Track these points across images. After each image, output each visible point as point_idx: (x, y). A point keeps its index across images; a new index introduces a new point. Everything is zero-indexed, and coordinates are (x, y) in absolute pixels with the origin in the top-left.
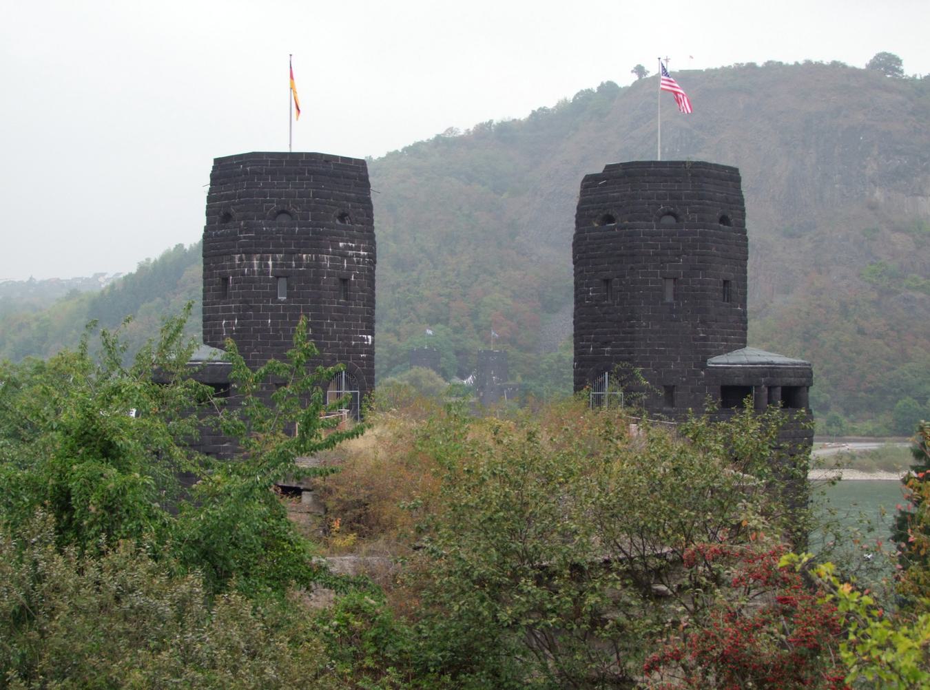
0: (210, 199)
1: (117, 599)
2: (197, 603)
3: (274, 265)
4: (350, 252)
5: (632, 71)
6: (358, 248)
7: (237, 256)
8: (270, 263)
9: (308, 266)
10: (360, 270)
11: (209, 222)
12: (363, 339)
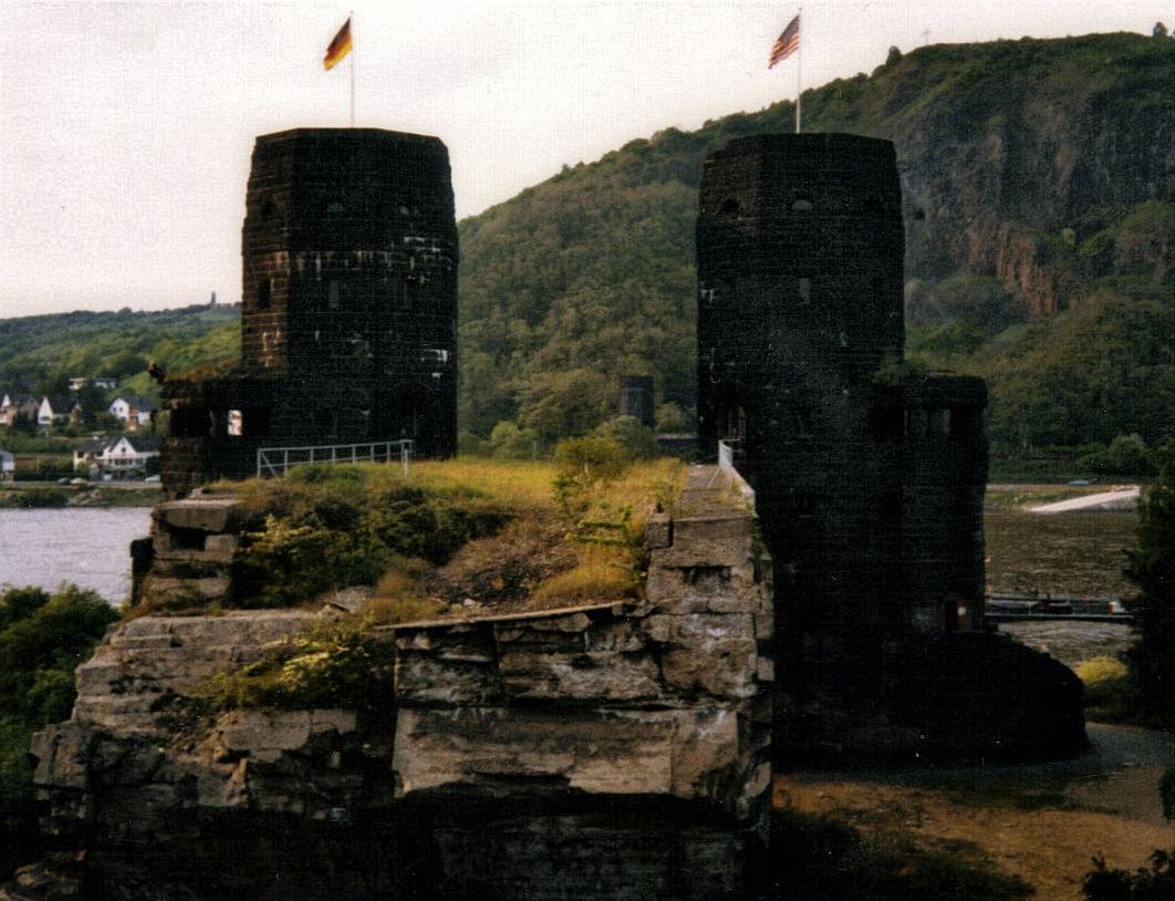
0: (251, 185)
1: (519, 243)
2: (176, 667)
3: (323, 265)
4: (418, 249)
5: (770, 67)
6: (428, 244)
7: (279, 254)
8: (318, 262)
9: (363, 265)
10: (433, 269)
11: (250, 212)
12: (435, 354)
